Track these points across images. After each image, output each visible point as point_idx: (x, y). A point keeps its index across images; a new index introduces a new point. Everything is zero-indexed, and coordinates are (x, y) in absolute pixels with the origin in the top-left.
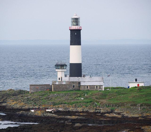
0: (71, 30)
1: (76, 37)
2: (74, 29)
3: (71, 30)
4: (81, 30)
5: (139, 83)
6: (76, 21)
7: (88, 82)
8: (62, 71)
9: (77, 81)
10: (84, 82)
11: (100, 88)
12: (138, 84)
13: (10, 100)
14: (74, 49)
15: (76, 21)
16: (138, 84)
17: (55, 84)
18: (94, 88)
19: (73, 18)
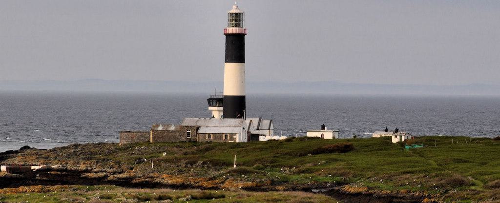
0: (228, 36)
1: (236, 49)
2: (230, 32)
3: (228, 36)
4: (246, 34)
5: (324, 133)
6: (237, 19)
7: (213, 128)
8: (218, 111)
9: (194, 125)
10: (207, 127)
11: (232, 138)
12: (322, 133)
13: (394, 167)
14: (231, 69)
15: (237, 19)
16: (322, 133)
17: (156, 129)
18: (221, 137)
19: (233, 14)
